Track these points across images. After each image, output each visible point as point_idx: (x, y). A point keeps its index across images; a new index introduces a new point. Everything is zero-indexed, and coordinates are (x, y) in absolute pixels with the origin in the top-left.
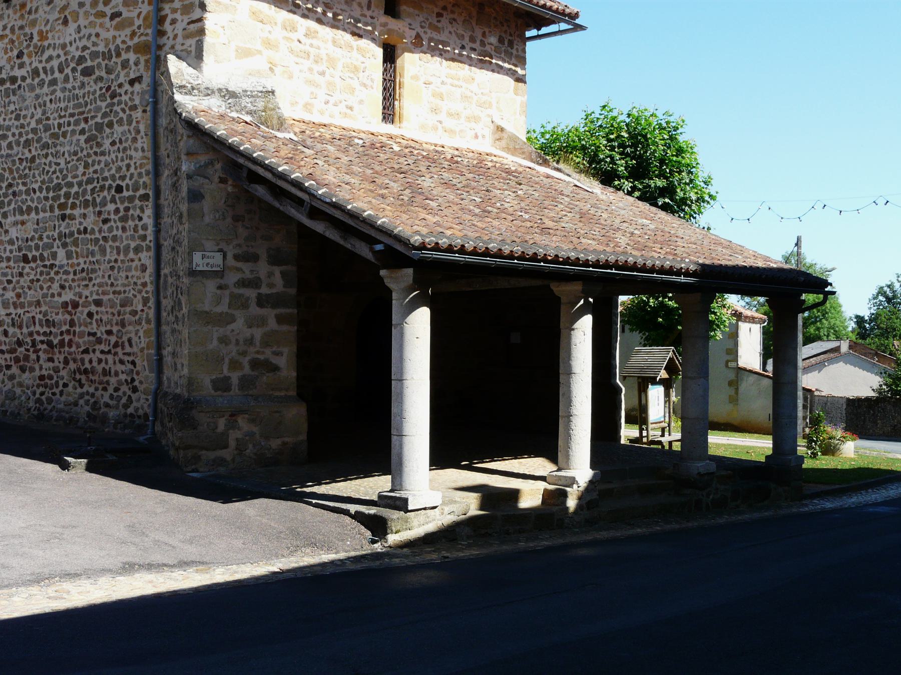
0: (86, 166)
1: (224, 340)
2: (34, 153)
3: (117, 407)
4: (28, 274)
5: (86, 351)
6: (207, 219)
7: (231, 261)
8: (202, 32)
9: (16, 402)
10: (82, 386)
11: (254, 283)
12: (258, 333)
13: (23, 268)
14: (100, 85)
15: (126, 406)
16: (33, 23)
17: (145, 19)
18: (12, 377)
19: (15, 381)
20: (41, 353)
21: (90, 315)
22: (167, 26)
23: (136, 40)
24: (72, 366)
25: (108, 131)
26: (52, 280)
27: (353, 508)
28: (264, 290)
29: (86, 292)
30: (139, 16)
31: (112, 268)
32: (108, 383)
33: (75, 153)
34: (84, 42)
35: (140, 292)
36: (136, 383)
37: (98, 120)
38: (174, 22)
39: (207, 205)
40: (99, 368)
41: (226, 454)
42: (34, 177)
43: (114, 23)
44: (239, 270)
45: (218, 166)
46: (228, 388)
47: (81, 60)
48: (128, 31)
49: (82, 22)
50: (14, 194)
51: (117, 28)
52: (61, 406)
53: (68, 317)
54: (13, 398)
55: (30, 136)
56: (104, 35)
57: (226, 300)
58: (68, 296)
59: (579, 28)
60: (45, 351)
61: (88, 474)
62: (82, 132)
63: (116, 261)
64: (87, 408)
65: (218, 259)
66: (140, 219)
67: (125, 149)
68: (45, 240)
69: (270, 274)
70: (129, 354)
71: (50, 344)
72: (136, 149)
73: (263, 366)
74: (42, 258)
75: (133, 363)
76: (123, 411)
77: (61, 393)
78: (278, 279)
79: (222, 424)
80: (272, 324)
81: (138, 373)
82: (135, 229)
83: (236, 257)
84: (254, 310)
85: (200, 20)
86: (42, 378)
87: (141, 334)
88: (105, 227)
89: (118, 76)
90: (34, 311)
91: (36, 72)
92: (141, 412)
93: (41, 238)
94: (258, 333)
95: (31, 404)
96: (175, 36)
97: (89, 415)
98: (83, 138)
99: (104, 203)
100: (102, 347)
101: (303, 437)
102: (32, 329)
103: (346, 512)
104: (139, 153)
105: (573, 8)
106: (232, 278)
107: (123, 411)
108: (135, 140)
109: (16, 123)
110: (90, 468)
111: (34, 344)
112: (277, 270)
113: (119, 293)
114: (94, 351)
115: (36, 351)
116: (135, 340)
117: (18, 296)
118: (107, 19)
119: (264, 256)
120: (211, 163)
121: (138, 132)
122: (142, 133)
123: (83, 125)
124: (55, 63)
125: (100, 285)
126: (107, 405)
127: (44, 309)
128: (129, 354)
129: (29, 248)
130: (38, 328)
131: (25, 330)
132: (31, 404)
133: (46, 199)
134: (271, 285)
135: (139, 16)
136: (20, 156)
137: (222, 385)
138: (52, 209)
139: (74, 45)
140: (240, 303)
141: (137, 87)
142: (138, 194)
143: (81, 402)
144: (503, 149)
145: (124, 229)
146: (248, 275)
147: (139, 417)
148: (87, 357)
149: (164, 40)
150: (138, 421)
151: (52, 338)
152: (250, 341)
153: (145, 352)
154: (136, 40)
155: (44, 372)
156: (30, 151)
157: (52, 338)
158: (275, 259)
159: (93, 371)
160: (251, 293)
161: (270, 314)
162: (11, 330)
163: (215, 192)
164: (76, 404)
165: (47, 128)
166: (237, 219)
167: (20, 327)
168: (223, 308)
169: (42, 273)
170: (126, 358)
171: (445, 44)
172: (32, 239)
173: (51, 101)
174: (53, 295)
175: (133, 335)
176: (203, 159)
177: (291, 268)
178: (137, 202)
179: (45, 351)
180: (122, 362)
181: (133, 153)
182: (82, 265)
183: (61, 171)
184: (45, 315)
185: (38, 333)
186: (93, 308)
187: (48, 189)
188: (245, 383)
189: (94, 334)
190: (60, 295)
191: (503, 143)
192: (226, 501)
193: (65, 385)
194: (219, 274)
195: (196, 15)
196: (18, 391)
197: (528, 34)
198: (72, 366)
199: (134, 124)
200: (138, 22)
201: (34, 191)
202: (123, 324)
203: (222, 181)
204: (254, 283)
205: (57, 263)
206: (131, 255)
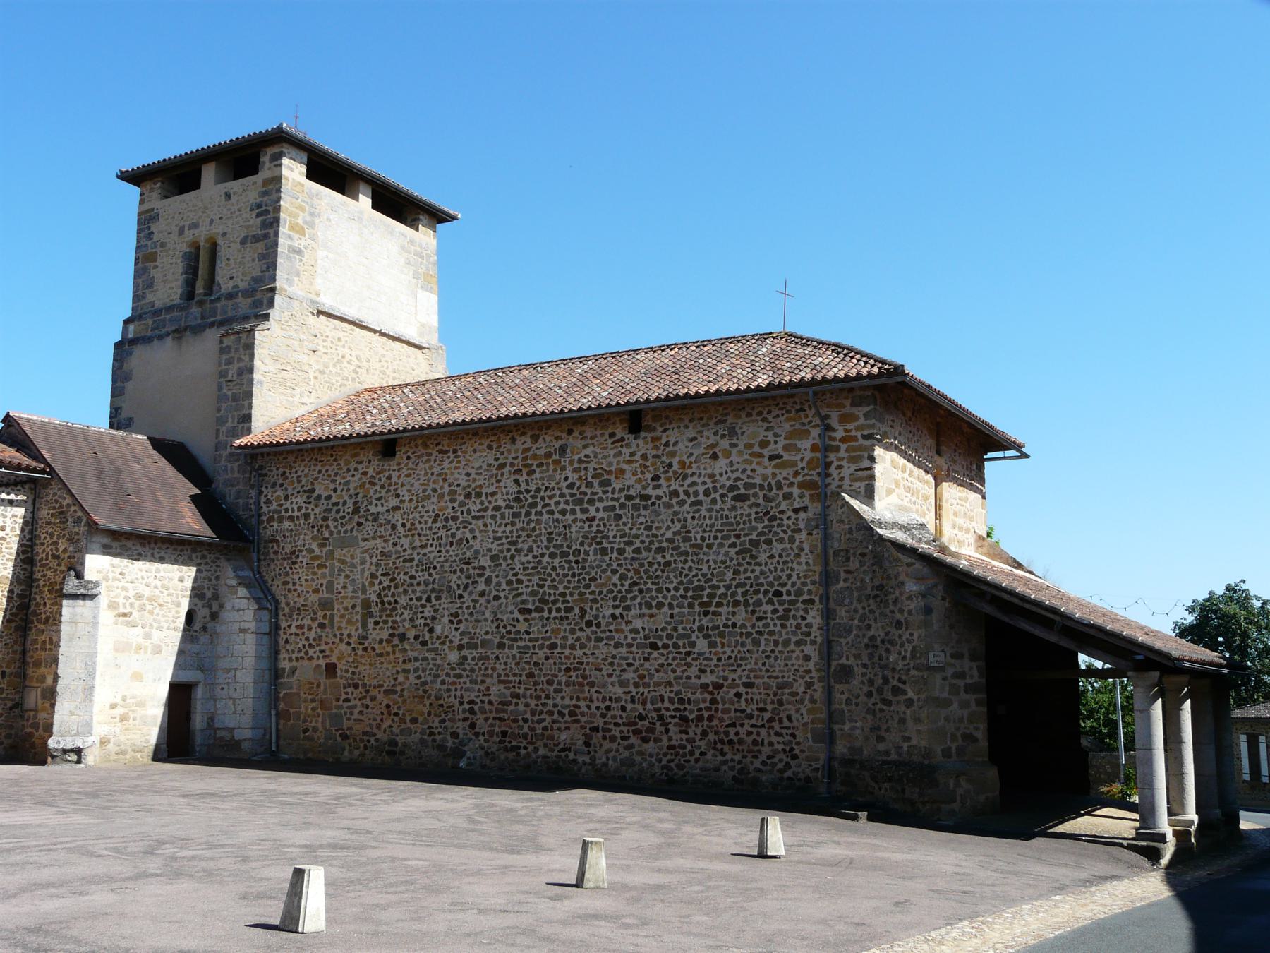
0: (736, 572)
1: (947, 719)
2: (668, 557)
3: (771, 772)
4: (656, 659)
5: (733, 725)
6: (936, 627)
7: (949, 659)
8: (872, 478)
9: (636, 768)
10: (723, 754)
11: (960, 675)
12: (966, 712)
13: (650, 654)
14: (755, 509)
15: (781, 771)
16: (673, 454)
17: (808, 463)
18: (631, 747)
19: (634, 751)
20: (670, 727)
21: (738, 695)
22: (832, 470)
23: (800, 478)
24: (712, 737)
25: (765, 546)
26: (689, 665)
27: (1125, 843)
28: (968, 681)
29: (732, 676)
30: (802, 459)
31: (768, 657)
32: (759, 751)
33: (723, 562)
34: (738, 474)
35: (802, 677)
36: (797, 752)
37: (754, 537)
38: (839, 467)
39: (935, 616)
40: (750, 740)
41: (956, 806)
42: (668, 577)
43: (773, 463)
44: (953, 665)
45: (941, 587)
46: (950, 756)
47: (732, 488)
48: (791, 471)
49: (734, 458)
50: (641, 591)
51: (776, 466)
52: (698, 771)
53: (709, 697)
54: (633, 763)
55: (665, 544)
56: (760, 470)
57: (947, 688)
58: (708, 678)
59: (1027, 456)
60: (676, 725)
61: (871, 823)
62: (733, 545)
63: (773, 651)
64: (732, 773)
65: (941, 657)
66: (804, 619)
67: (785, 563)
68: (680, 631)
69: (971, 668)
70: (788, 728)
71: (684, 719)
72: (799, 563)
73: (969, 738)
74: (675, 646)
75: (793, 735)
76: (778, 775)
77: (697, 760)
78: (975, 673)
79: (952, 784)
80: (974, 707)
81: (798, 743)
82: (798, 626)
83: (952, 656)
84: (964, 696)
85: (871, 468)
86: (671, 747)
87: (804, 711)
88: (761, 623)
89: (779, 504)
90: (661, 690)
91: (675, 493)
92: (801, 776)
93: (675, 629)
94: (966, 712)
95: (657, 769)
96: (842, 479)
97: (734, 778)
98: (733, 551)
99: (758, 603)
100: (754, 721)
101: (997, 793)
102: (660, 705)
103: (1121, 845)
104: (804, 566)
105: (1020, 440)
106: (950, 671)
107: (778, 775)
108: (798, 556)
109: (646, 533)
110: (870, 819)
111: (661, 718)
112: (974, 665)
113: (777, 677)
114: (742, 725)
115: (665, 724)
116: (795, 716)
117: (642, 677)
118: (766, 460)
119: (967, 655)
120: (935, 586)
121: (802, 550)
122: (807, 551)
123: (733, 540)
124: (701, 489)
125: (750, 670)
126: (759, 770)
127: (675, 688)
128: (788, 728)
129: (661, 638)
130: (667, 704)
131: (649, 706)
132: (657, 769)
133: (685, 597)
134: (972, 677)
135: (802, 459)
136: (650, 559)
137: (947, 753)
138: (691, 606)
139: (725, 477)
140: (954, 690)
141: (802, 515)
142: (801, 599)
143: (724, 768)
144: (985, 555)
145: (783, 626)
146: (959, 670)
147: (799, 780)
148: (732, 731)
149: (829, 480)
150: (798, 784)
151: (686, 713)
152: (961, 720)
153: (810, 726)
154: (800, 478)
155: (674, 742)
156: (664, 557)
157: (686, 713)
158: (973, 658)
159: (741, 742)
160: (960, 683)
161: (971, 698)
162: (629, 706)
163: (939, 604)
164: (717, 769)
165: (686, 539)
166: (951, 627)
167: (644, 703)
168: (945, 695)
169: (674, 659)
170: (784, 731)
171: (957, 473)
172: (663, 629)
173: (693, 518)
174: (689, 677)
175: (793, 712)
176: (930, 582)
177: (982, 664)
178: (799, 604)
179: (676, 725)
180: (777, 734)
181: (795, 565)
182: (729, 653)
183: (704, 575)
184: (678, 693)
185: (667, 709)
186: (742, 690)
187: (686, 590)
188: (961, 751)
189: (743, 711)
190: (699, 677)
191: (985, 549)
192: (1027, 840)
193: (702, 754)
194: (942, 669)
195: (866, 464)
196: (638, 759)
197: (990, 455)
198: (712, 737)
199: (797, 543)
200: (800, 465)
201: (668, 590)
202: (780, 703)
203: (943, 599)
204: (960, 675)
205: (696, 650)
206: (792, 647)
